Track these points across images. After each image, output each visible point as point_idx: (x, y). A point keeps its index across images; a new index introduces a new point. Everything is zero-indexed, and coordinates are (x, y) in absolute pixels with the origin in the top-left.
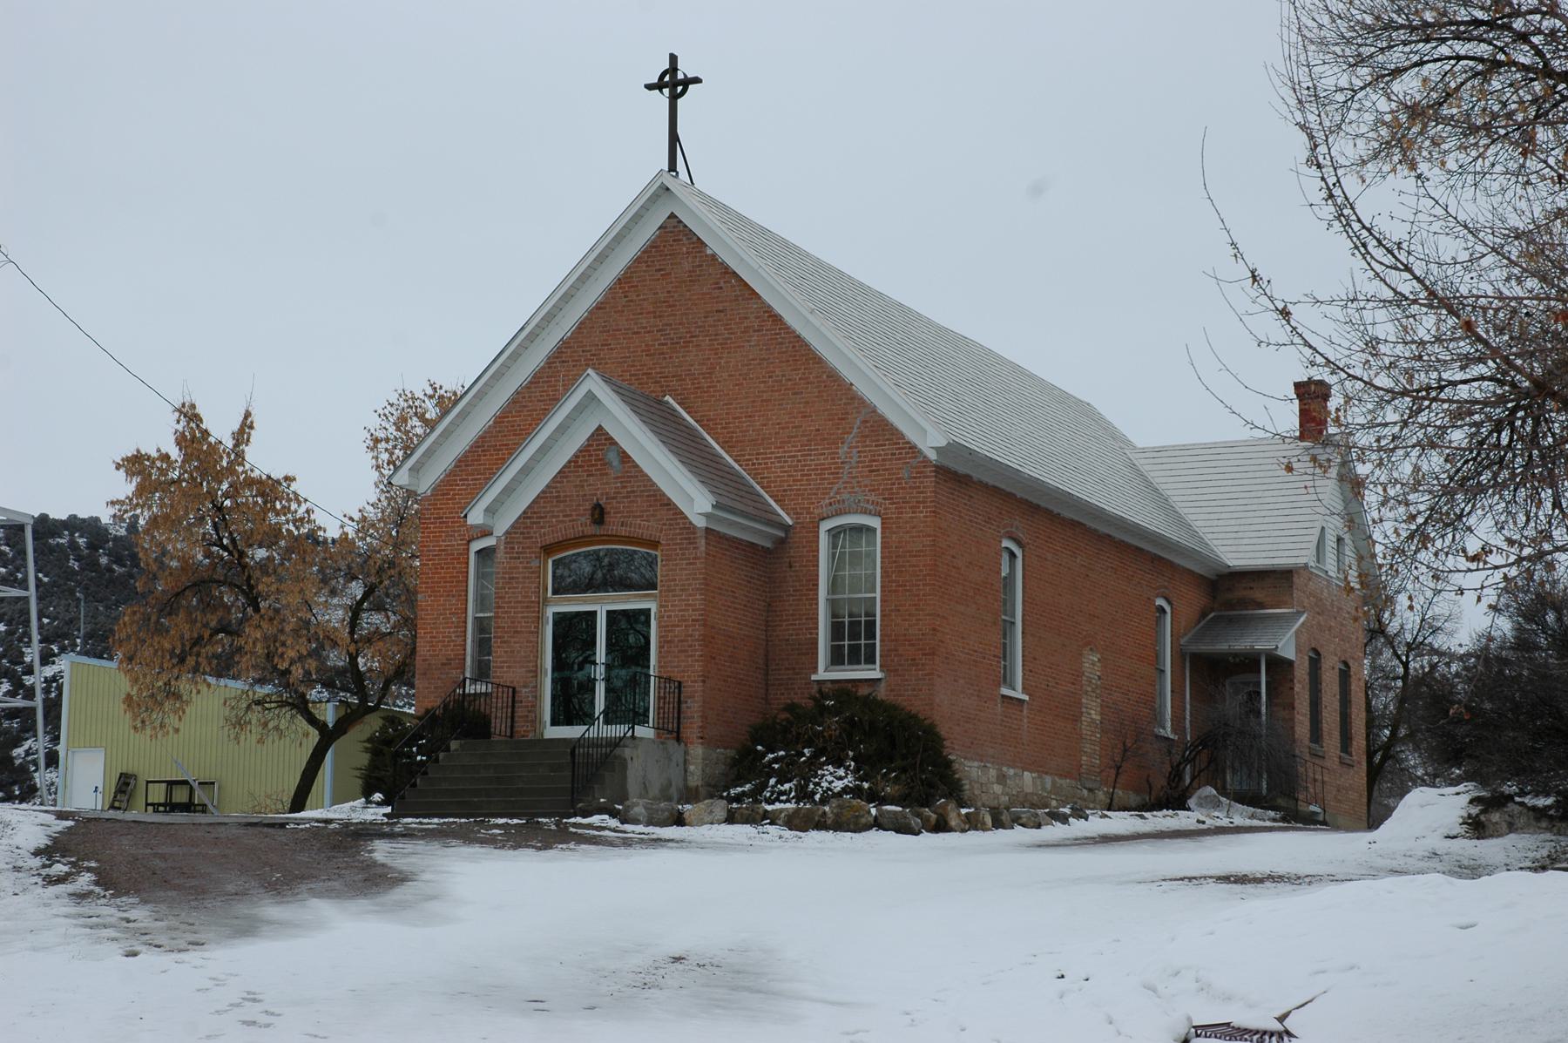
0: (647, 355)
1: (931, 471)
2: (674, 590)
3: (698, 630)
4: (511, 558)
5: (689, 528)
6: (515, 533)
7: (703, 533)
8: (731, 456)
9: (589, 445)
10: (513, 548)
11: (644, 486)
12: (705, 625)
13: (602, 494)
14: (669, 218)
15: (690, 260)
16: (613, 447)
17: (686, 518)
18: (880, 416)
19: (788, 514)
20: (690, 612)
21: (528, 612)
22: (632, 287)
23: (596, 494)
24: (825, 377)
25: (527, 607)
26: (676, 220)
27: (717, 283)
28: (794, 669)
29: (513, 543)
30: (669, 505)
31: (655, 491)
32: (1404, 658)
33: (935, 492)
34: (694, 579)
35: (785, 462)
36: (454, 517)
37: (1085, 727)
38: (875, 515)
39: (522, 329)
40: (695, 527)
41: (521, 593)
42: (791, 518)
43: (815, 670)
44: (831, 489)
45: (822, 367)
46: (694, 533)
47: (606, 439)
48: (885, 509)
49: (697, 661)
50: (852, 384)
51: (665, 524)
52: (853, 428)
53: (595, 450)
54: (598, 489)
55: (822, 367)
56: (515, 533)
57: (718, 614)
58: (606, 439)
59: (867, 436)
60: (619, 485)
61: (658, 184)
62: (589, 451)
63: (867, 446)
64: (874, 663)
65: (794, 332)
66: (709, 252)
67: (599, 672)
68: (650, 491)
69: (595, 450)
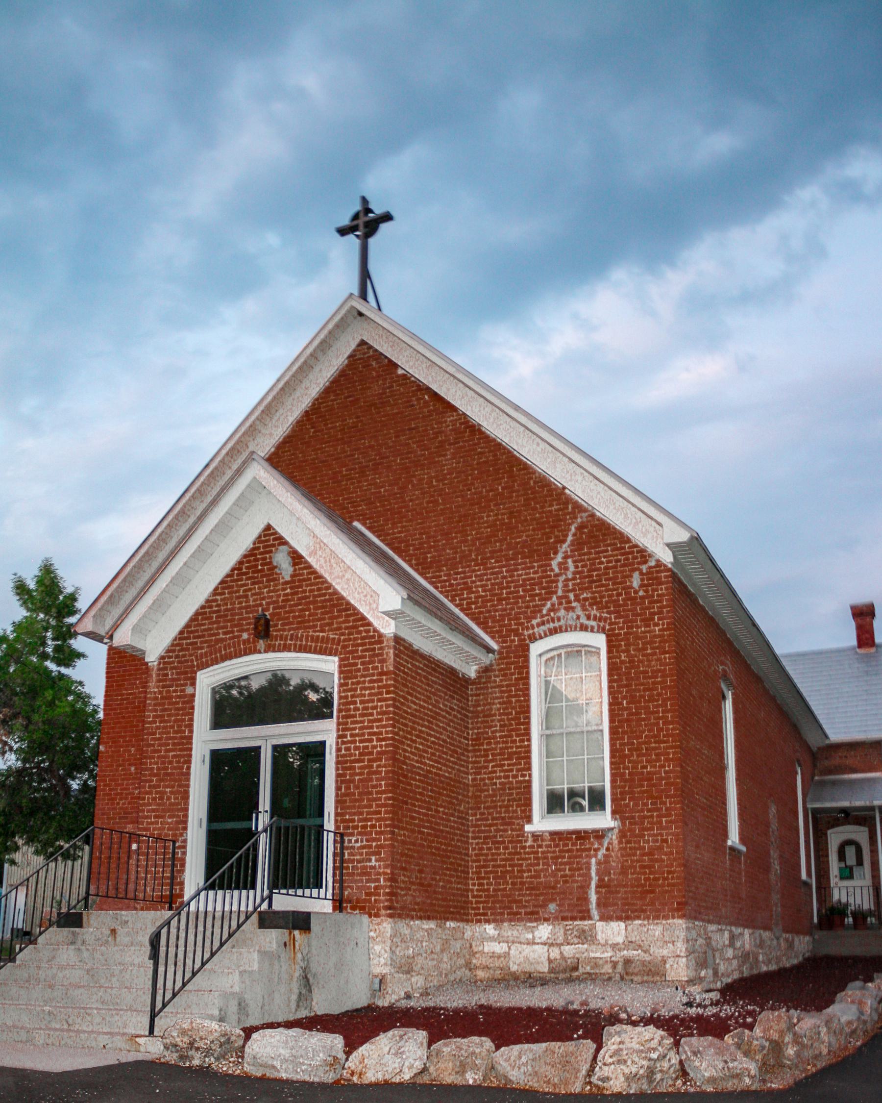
0: (334, 483)
1: (666, 577)
2: (354, 716)
3: (385, 766)
4: (163, 687)
5: (373, 637)
6: (170, 657)
7: (392, 644)
8: (426, 578)
9: (253, 549)
10: (167, 675)
11: (319, 589)
12: (394, 759)
13: (268, 604)
14: (359, 345)
15: (380, 382)
16: (282, 548)
17: (369, 624)
18: (599, 519)
19: (493, 638)
20: (375, 743)
21: (180, 750)
22: (321, 417)
23: (261, 605)
24: (532, 482)
25: (179, 744)
26: (365, 347)
27: (408, 402)
28: (503, 818)
29: (166, 669)
30: (348, 609)
31: (330, 594)
32: (26, 883)
33: (391, 894)
34: (379, 700)
35: (487, 580)
36: (136, 665)
37: (772, 877)
38: (598, 632)
39: (207, 466)
40: (381, 635)
41: (172, 727)
42: (497, 642)
43: (529, 820)
44: (544, 605)
45: (530, 473)
46: (381, 642)
47: (274, 539)
48: (611, 624)
49: (385, 805)
50: (564, 488)
51: (343, 634)
52: (567, 535)
53: (261, 553)
54: (263, 599)
55: (530, 473)
56: (170, 657)
57: (411, 747)
58: (274, 539)
59: (584, 543)
60: (288, 591)
61: (346, 308)
62: (255, 555)
63: (584, 554)
64: (603, 808)
65: (494, 440)
66: (400, 372)
67: (263, 820)
68: (325, 595)
69: (261, 553)
